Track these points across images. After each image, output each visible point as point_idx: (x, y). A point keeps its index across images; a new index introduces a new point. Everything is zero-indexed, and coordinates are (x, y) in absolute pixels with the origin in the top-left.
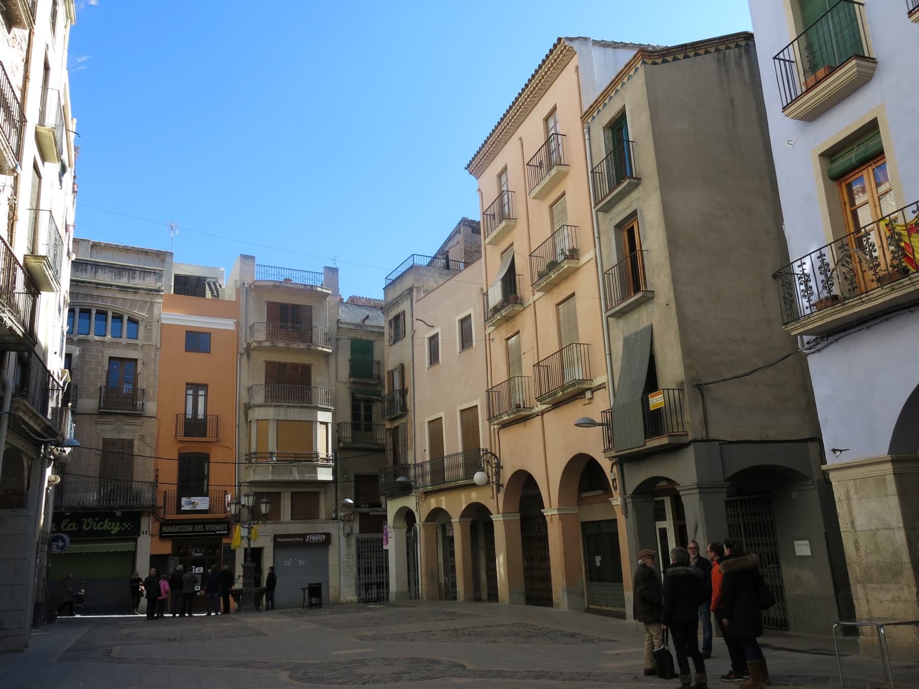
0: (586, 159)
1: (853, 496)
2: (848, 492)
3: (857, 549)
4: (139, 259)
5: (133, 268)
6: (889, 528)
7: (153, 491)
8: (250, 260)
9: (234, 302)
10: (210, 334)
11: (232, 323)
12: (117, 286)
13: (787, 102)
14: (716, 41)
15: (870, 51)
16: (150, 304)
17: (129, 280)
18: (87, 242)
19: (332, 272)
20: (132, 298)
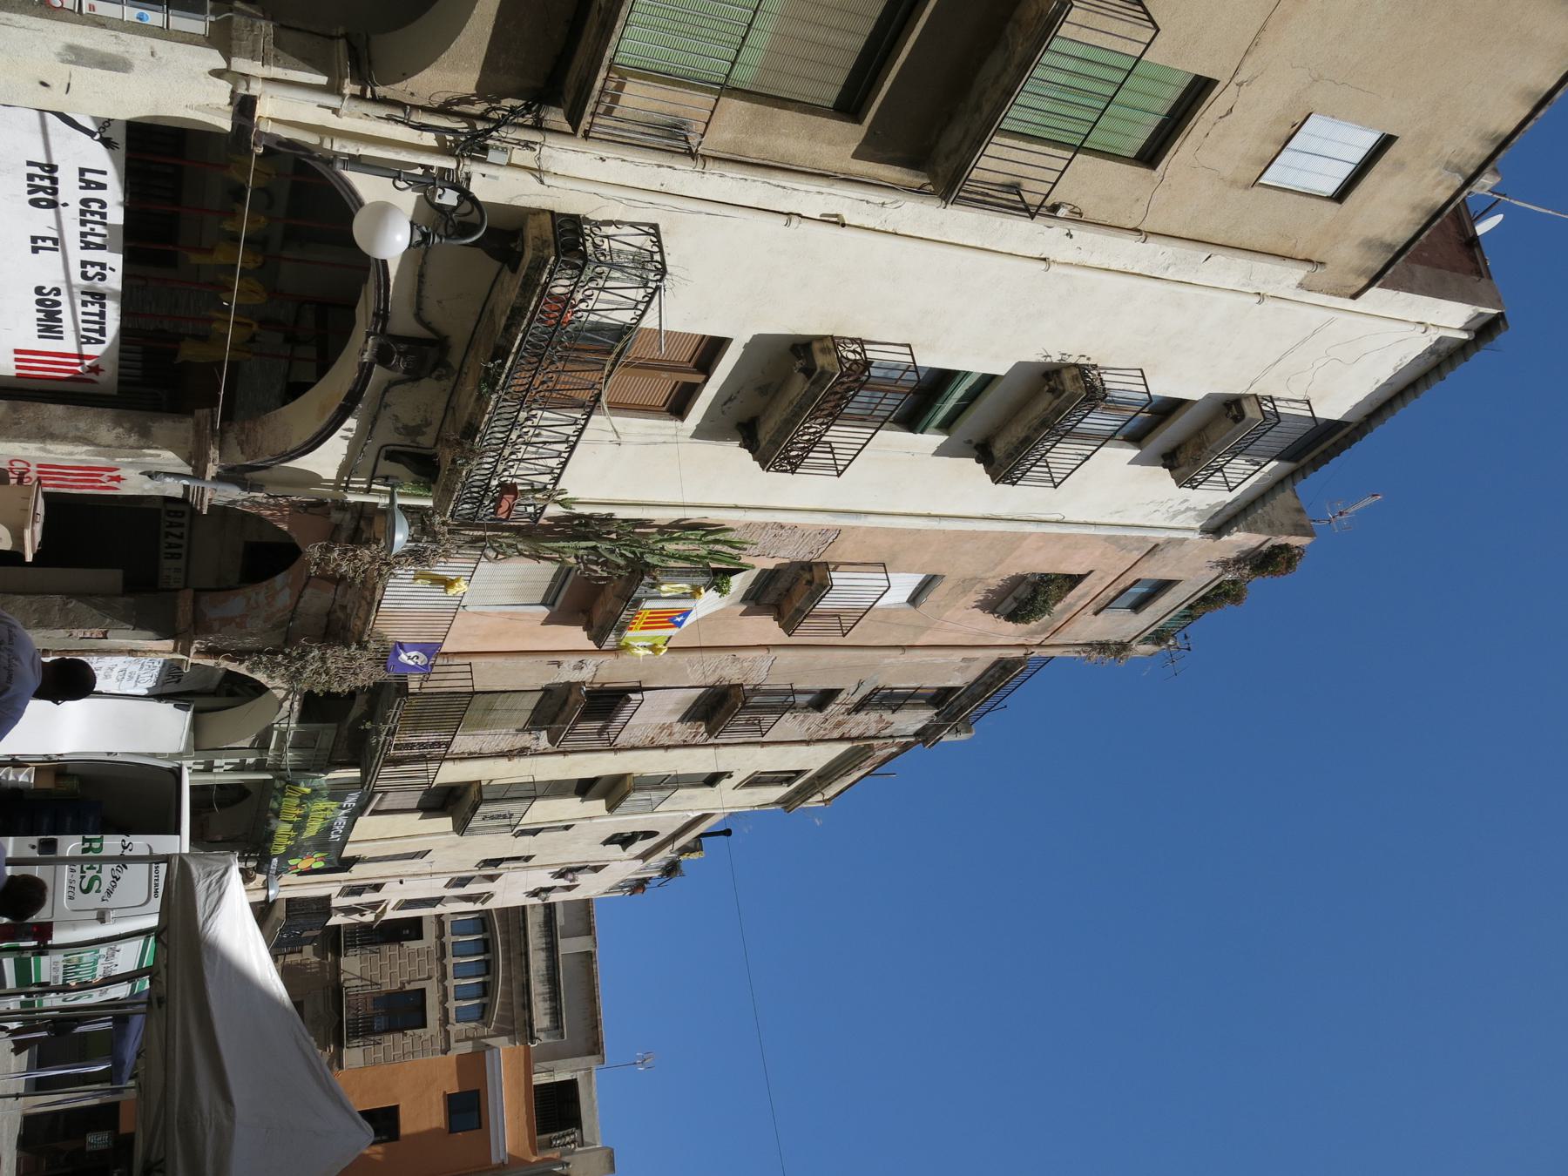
4: (586, 1019)
5: (558, 997)
8: (607, 1165)
9: (114, 396)
10: (480, 1127)
11: (502, 1157)
12: (528, 980)
16: (511, 1030)
17: (540, 994)
18: (592, 944)
20: (515, 1004)
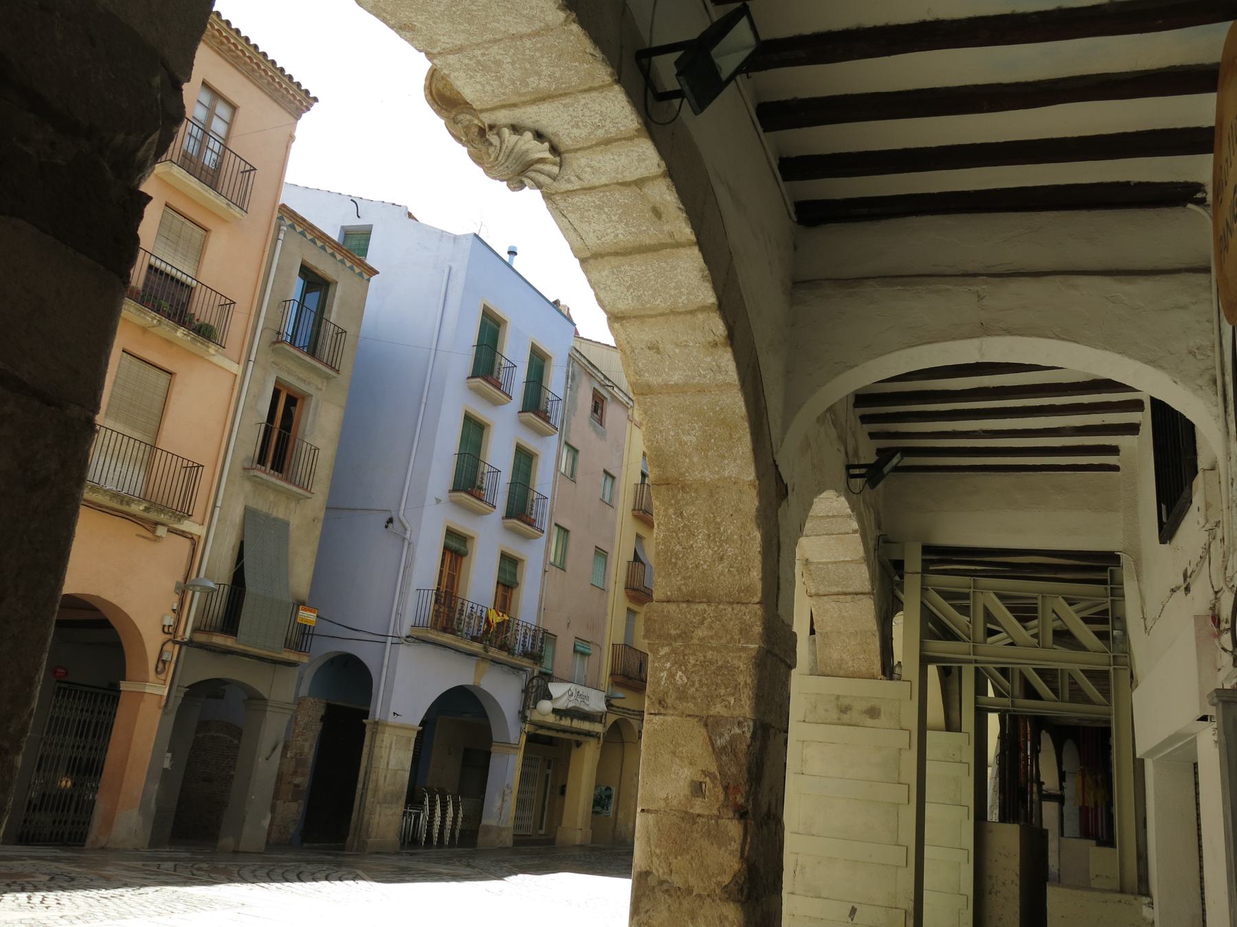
0: (214, 474)
1: (393, 746)
2: (392, 742)
3: (385, 780)
6: (404, 770)
7: (528, 101)
13: (250, 173)
14: (332, 243)
15: (444, 315)
19: (748, 77)
